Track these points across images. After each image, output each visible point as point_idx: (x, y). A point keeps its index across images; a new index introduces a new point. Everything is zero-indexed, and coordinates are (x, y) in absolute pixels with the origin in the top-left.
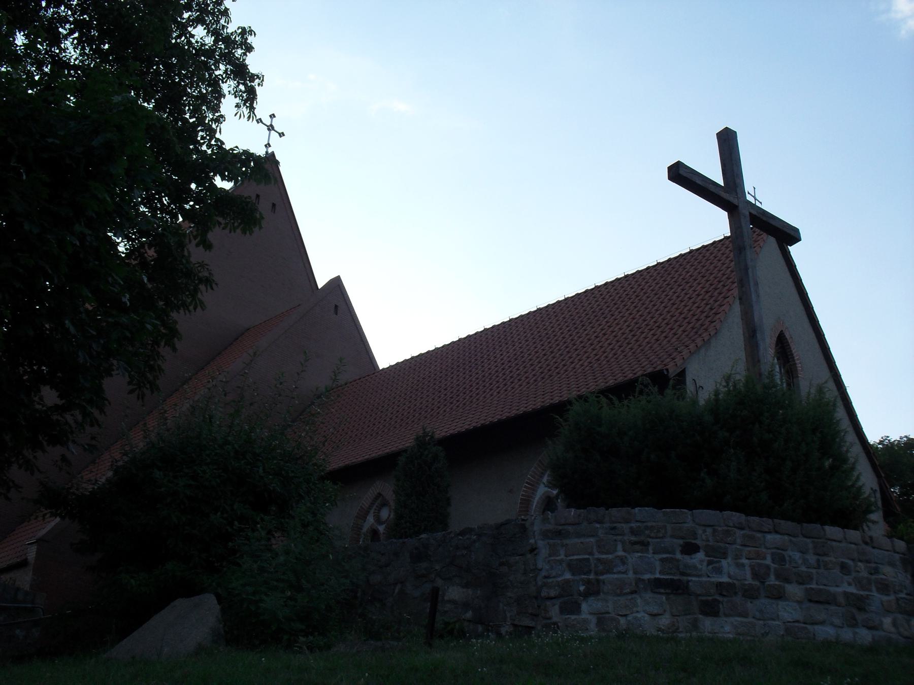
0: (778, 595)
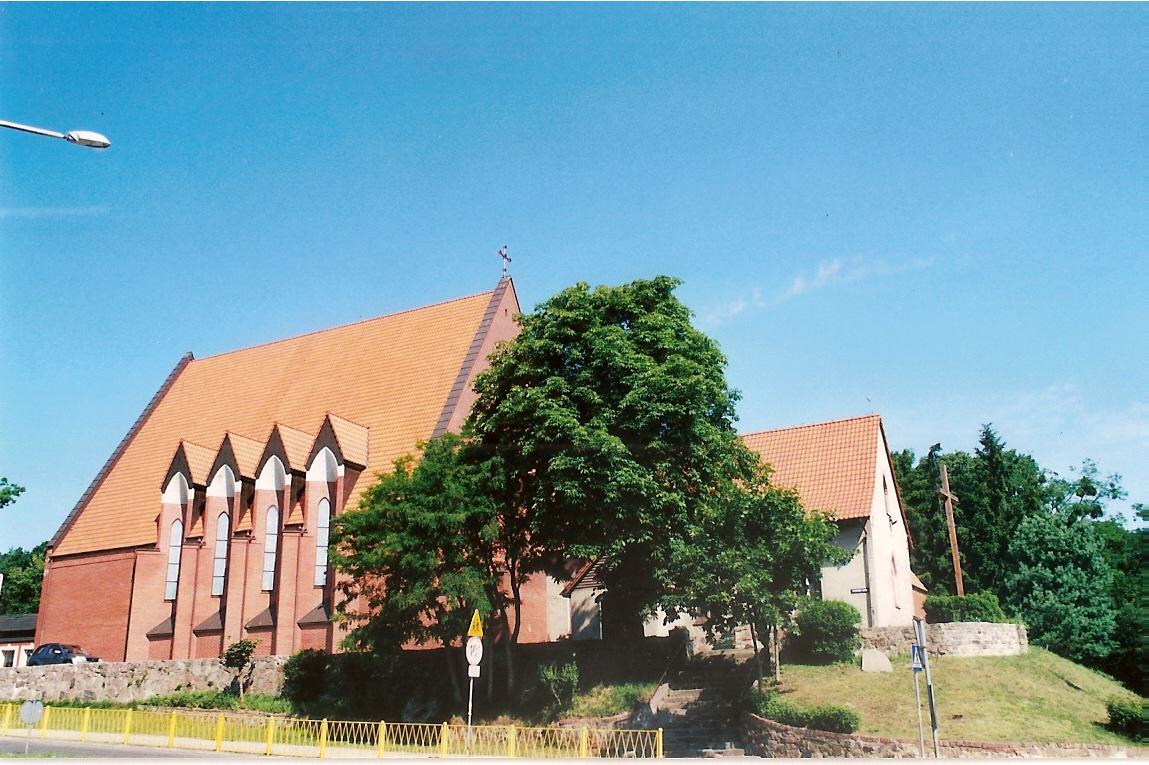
0: (996, 643)
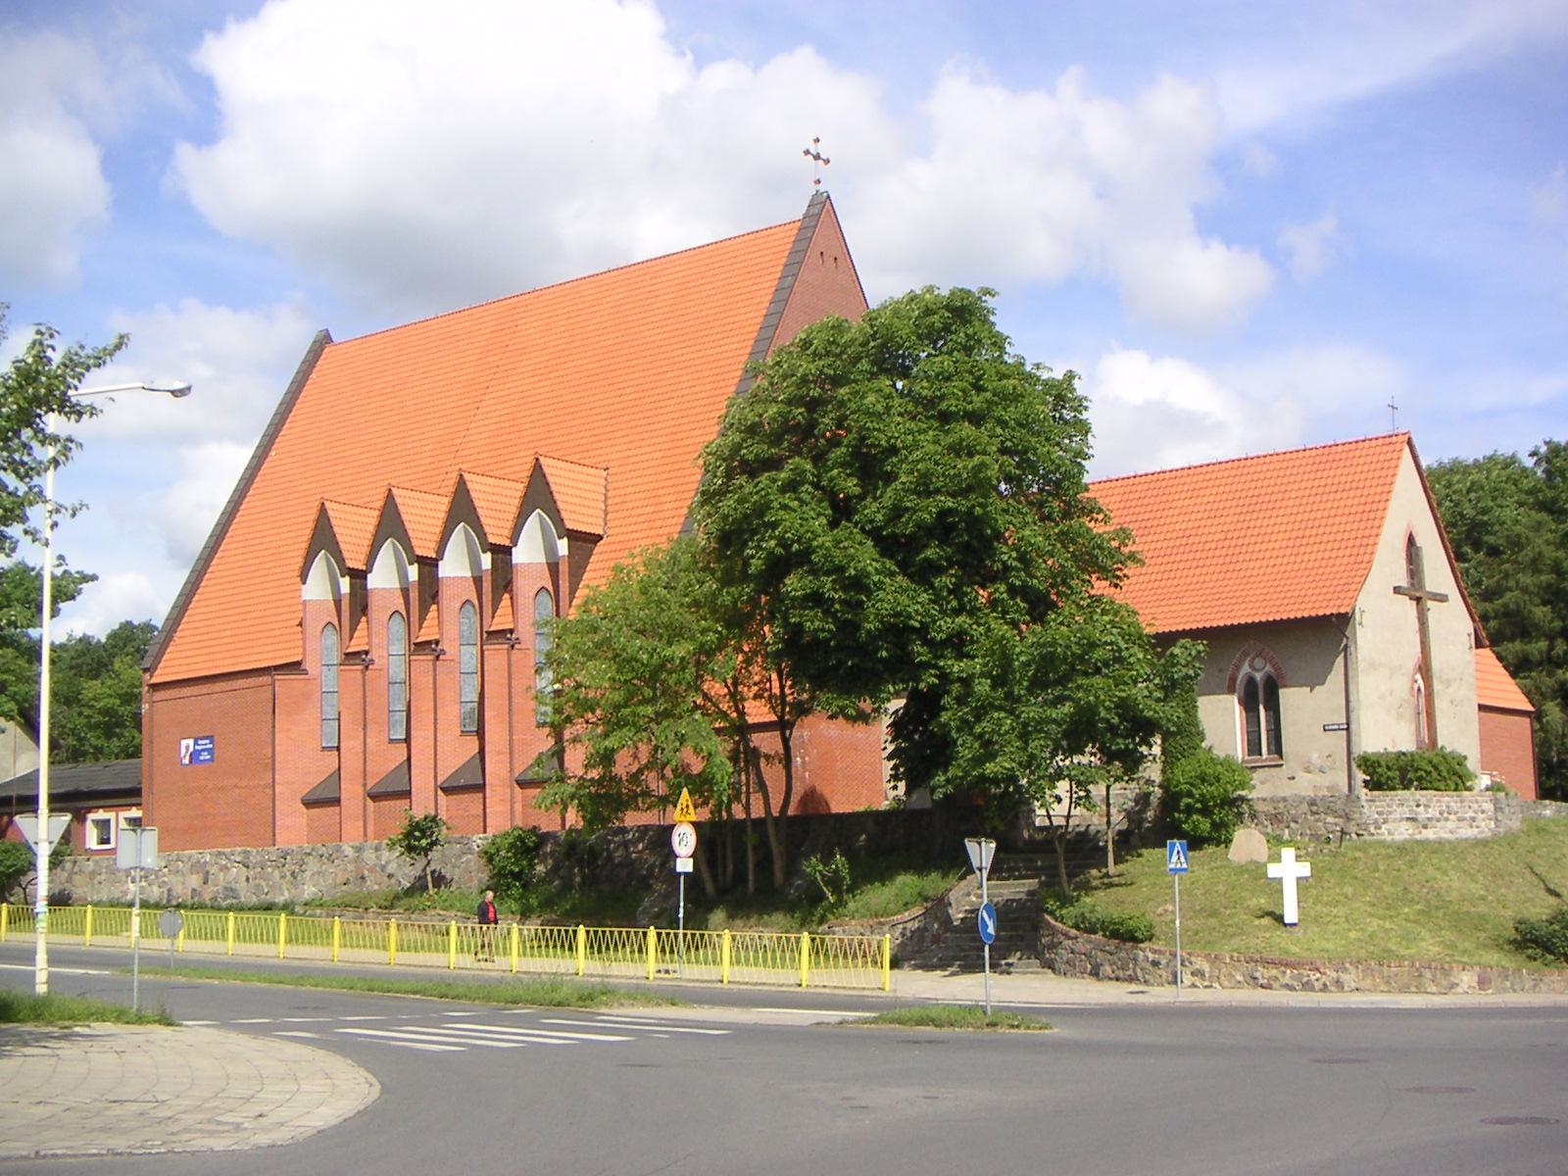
0: (1447, 819)
